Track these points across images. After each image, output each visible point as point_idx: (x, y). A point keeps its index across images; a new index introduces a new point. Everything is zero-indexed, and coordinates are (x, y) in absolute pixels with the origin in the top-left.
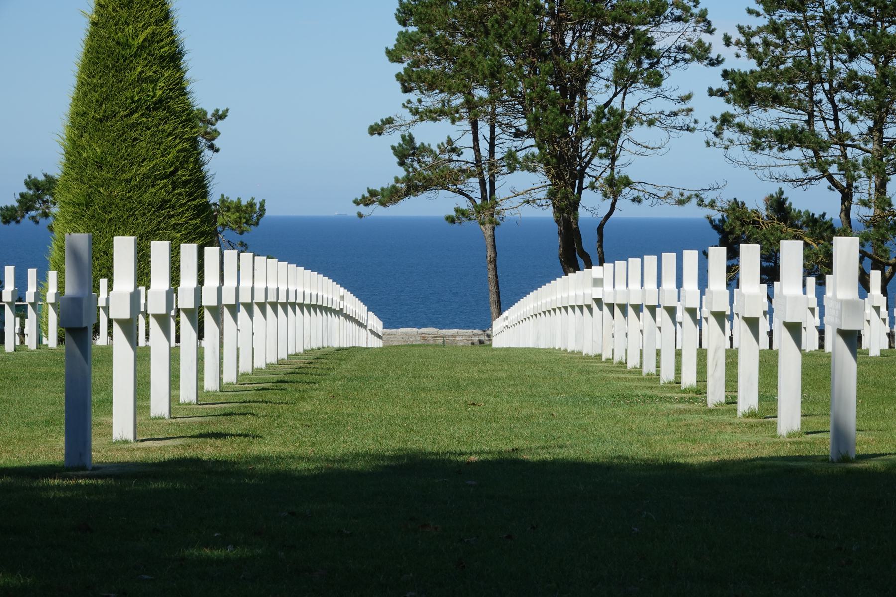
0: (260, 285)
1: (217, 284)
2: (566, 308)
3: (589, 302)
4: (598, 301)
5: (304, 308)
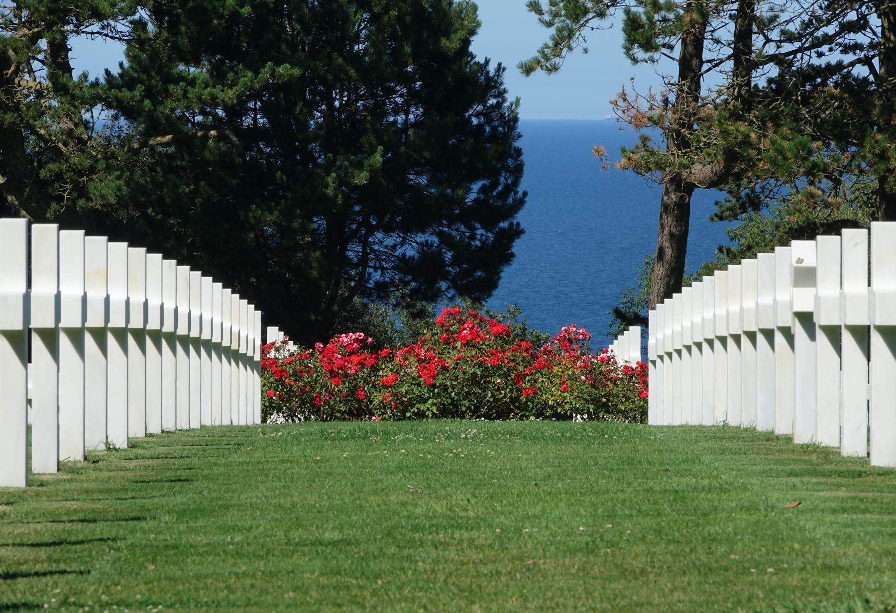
0: (71, 292)
1: (23, 289)
2: (723, 340)
3: (788, 320)
4: (806, 319)
5: (178, 344)
